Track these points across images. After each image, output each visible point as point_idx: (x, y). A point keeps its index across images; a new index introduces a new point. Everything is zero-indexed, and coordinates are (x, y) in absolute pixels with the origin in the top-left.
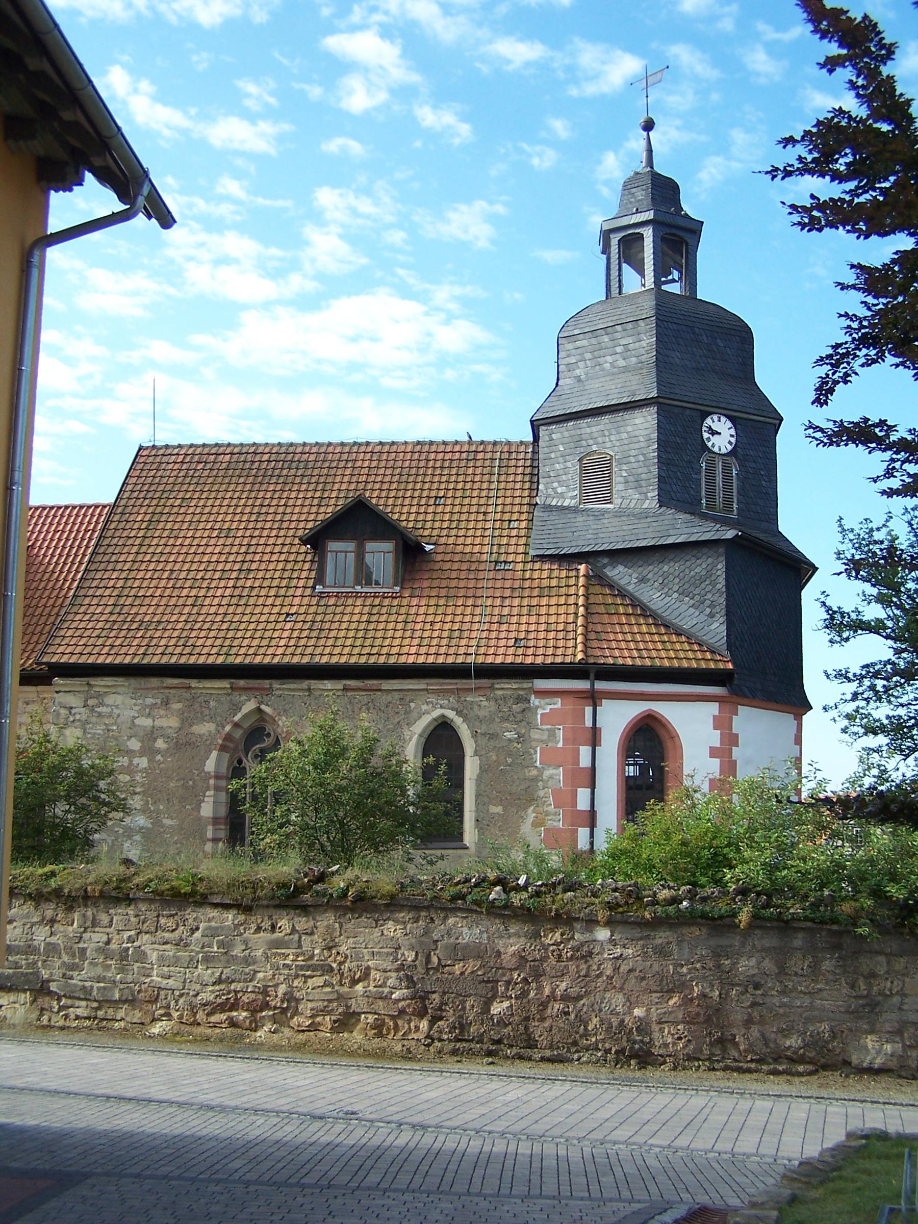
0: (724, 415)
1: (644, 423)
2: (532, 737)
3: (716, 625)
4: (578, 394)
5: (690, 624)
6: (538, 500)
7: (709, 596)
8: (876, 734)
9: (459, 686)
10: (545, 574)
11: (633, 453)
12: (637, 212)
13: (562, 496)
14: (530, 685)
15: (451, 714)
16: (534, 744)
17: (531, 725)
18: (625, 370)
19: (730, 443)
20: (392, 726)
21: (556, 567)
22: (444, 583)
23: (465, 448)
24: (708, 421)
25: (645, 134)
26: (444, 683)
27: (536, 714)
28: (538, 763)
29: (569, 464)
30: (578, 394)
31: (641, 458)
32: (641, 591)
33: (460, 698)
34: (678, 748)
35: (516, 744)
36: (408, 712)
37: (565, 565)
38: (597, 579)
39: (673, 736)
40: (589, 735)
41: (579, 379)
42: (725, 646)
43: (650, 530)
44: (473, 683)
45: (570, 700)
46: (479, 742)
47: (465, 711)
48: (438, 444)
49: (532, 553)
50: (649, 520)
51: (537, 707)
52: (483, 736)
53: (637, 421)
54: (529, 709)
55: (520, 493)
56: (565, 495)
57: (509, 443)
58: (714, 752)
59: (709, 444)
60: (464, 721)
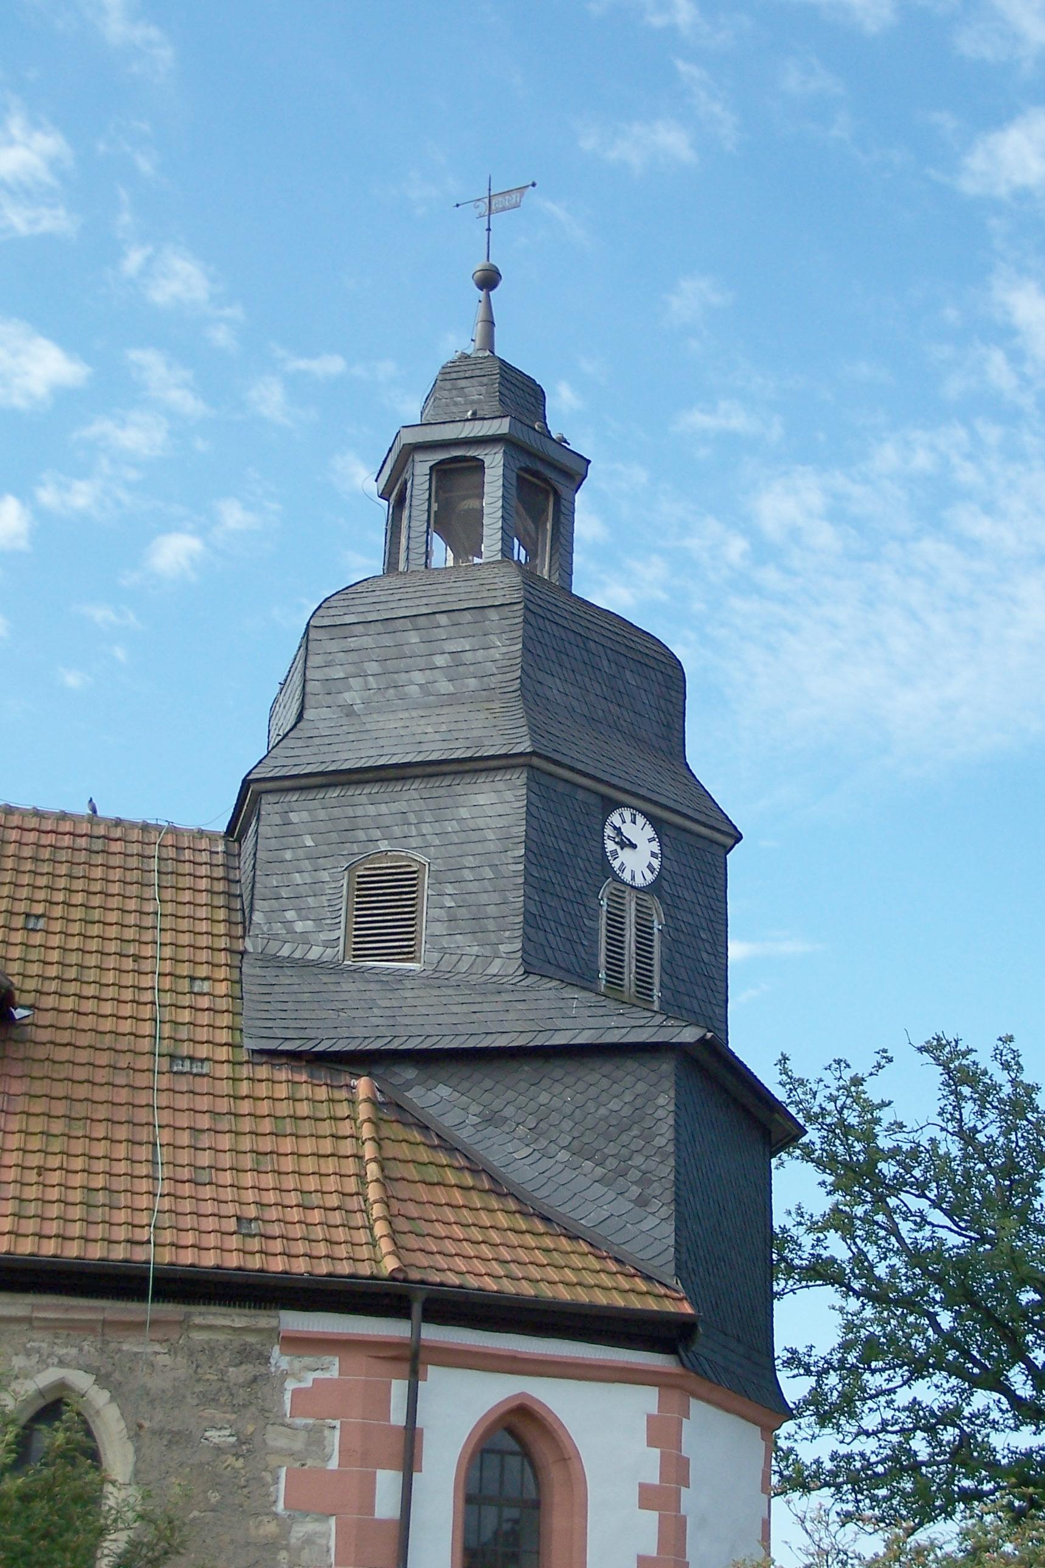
0: (645, 814)
1: (496, 809)
2: (270, 1443)
3: (650, 1223)
4: (351, 737)
5: (594, 1217)
6: (249, 944)
7: (638, 1160)
8: (806, 1489)
9: (109, 1315)
10: (282, 1091)
11: (470, 861)
12: (475, 418)
13: (304, 939)
14: (274, 1323)
15: (81, 1381)
16: (273, 1460)
17: (267, 1415)
18: (453, 700)
19: (650, 867)
21: (304, 1078)
22: (59, 1090)
23: (84, 828)
24: (615, 819)
25: (482, 294)
26: (73, 1307)
27: (282, 1391)
28: (280, 1507)
29: (325, 876)
30: (351, 737)
31: (488, 873)
32: (488, 1143)
33: (106, 1343)
34: (576, 1483)
35: (231, 1460)
37: (323, 1075)
38: (391, 1109)
39: (567, 1457)
40: (397, 1445)
41: (349, 711)
42: (671, 1268)
43: (511, 1016)
44: (149, 1310)
45: (360, 1360)
47: (117, 1376)
48: (24, 813)
49: (250, 1044)
50: (506, 997)
51: (285, 1375)
52: (158, 1438)
53: (481, 799)
54: (267, 1377)
55: (209, 924)
56: (312, 938)
57: (173, 830)
58: (648, 1497)
59: (616, 864)
60: (113, 1399)
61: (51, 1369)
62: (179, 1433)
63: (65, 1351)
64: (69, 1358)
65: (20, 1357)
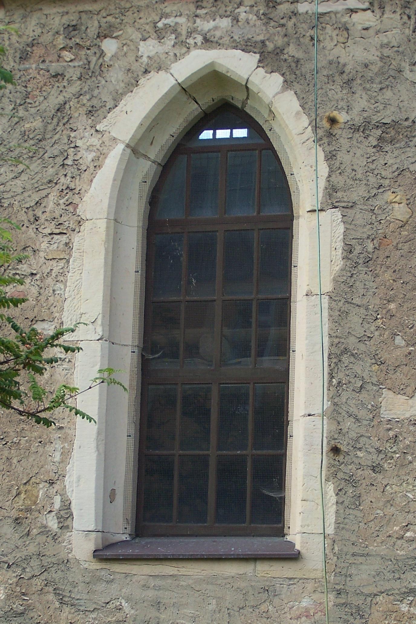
15: (241, 65)
20: (38, 123)
36: (93, 72)
46: (343, 157)
47: (292, 50)
60: (287, 84)
61: (195, 53)
62: (395, 124)
63: (212, 24)
64: (218, 34)
65: (150, 42)
